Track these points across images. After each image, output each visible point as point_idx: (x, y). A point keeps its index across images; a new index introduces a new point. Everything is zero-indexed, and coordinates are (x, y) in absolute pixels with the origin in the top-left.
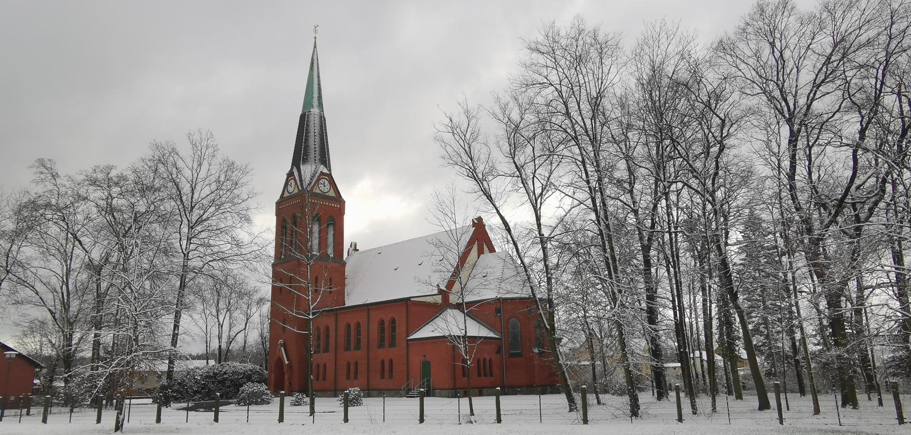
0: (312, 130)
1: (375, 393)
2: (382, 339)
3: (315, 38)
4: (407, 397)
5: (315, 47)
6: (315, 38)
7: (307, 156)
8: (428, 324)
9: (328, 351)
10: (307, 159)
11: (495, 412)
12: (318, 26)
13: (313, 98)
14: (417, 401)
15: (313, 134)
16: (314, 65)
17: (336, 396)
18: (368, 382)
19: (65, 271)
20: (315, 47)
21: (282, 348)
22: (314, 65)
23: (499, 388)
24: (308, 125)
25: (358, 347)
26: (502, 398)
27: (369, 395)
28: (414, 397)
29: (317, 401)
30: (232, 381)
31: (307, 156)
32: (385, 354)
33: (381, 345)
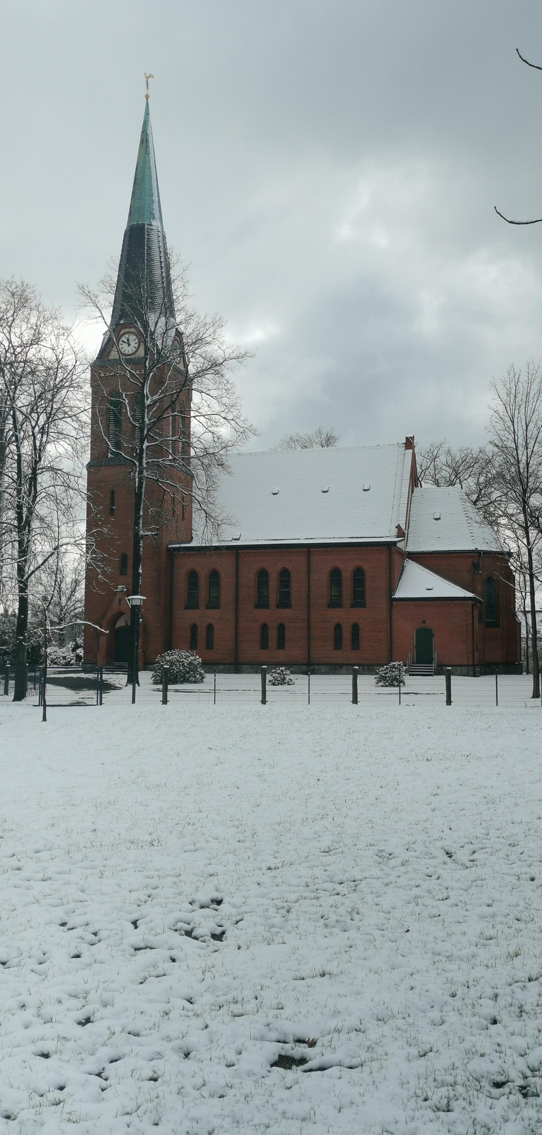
1: (323, 668)
3: (147, 97)
4: (410, 675)
5: (147, 114)
6: (147, 97)
12: (151, 76)
13: (153, 202)
20: (147, 114)
24: (149, 248)
28: (432, 675)
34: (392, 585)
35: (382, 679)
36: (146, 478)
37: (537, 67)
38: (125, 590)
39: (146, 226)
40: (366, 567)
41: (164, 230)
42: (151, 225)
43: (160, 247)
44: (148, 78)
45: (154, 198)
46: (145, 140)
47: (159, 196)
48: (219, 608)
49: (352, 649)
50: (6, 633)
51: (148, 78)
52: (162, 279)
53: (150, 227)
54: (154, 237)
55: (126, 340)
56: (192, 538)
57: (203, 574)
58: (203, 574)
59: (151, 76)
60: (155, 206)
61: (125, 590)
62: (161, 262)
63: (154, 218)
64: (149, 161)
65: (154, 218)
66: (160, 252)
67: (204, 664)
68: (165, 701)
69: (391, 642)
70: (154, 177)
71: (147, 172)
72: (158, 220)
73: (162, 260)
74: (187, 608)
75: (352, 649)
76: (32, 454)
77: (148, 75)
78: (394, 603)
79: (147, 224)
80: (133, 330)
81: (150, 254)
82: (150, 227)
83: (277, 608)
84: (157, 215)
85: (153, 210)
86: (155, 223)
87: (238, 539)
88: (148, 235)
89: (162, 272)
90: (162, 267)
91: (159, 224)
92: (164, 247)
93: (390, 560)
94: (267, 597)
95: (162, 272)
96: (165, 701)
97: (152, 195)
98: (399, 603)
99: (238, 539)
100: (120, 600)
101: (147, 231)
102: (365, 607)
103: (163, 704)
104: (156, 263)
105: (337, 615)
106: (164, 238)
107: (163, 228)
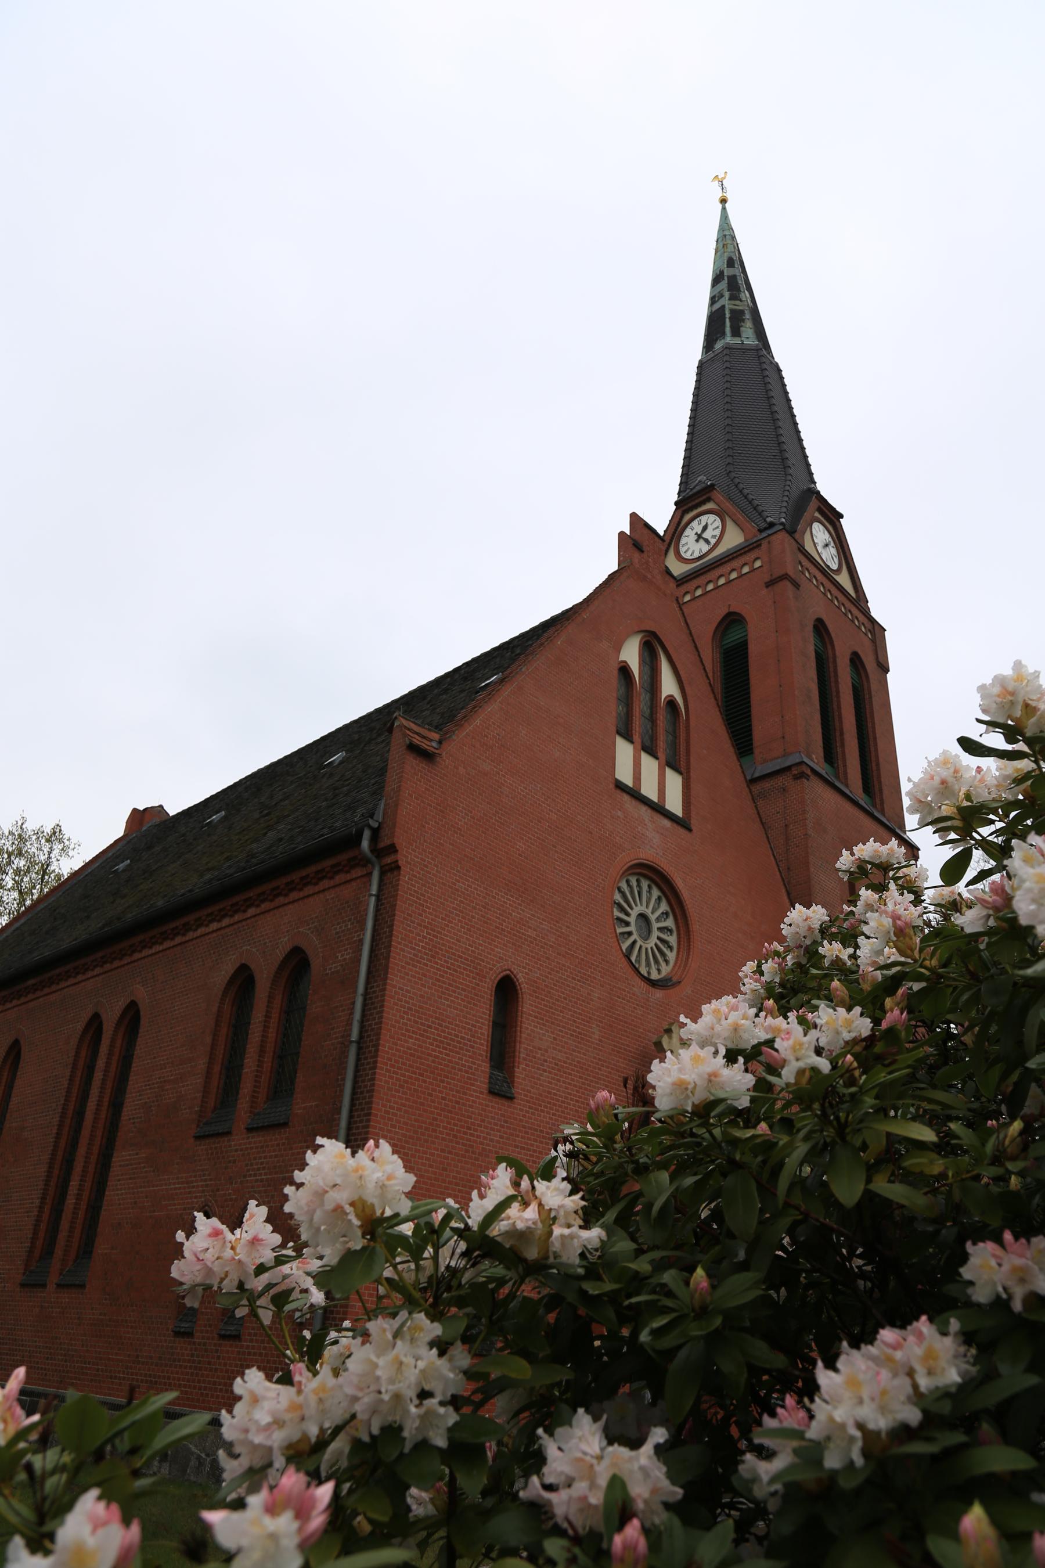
3: (723, 201)
16: (726, 238)
22: (726, 238)
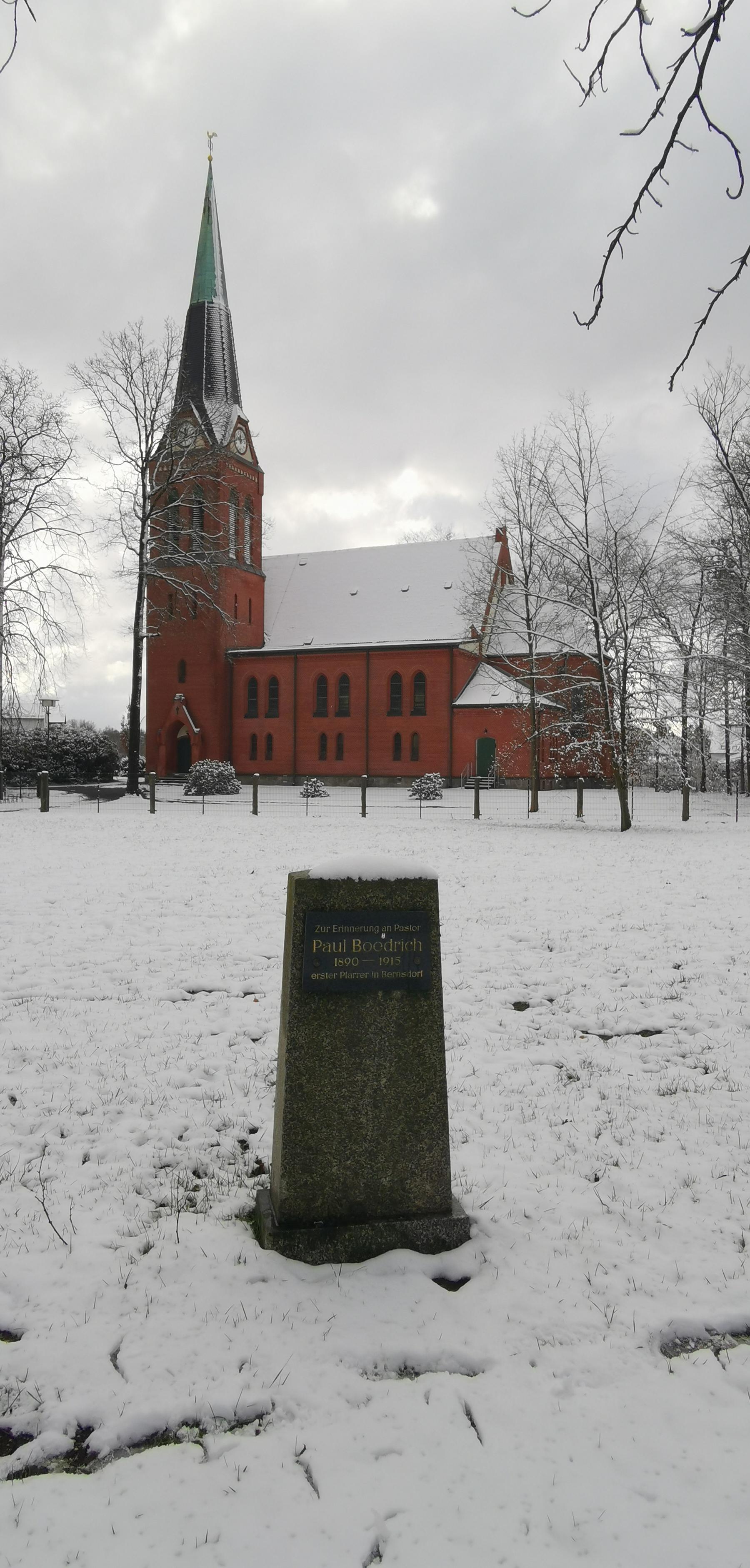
0: (218, 339)
1: (382, 781)
2: (253, 704)
3: (210, 159)
4: (466, 788)
5: (210, 178)
6: (210, 159)
7: (212, 383)
8: (468, 684)
9: (276, 715)
10: (212, 389)
11: (619, 812)
12: (214, 135)
13: (215, 277)
14: (472, 792)
15: (220, 345)
17: (296, 783)
18: (367, 766)
19: (144, 449)
20: (210, 178)
21: (184, 707)
23: (258, 775)
24: (210, 328)
25: (273, 710)
26: (586, 793)
27: (449, 785)
28: (487, 788)
29: (586, 793)
30: (75, 755)
31: (212, 385)
32: (404, 724)
33: (394, 708)
34: (455, 690)
35: (416, 792)
36: (148, 575)
37: (33, 15)
38: (183, 698)
39: (206, 304)
40: (427, 672)
41: (230, 307)
42: (212, 303)
43: (221, 326)
44: (211, 137)
45: (216, 273)
46: (207, 209)
47: (223, 271)
48: (278, 717)
49: (411, 760)
50: (68, 743)
51: (211, 137)
52: (224, 361)
53: (211, 305)
54: (215, 316)
55: (183, 431)
56: (264, 643)
57: (263, 680)
58: (263, 680)
59: (214, 135)
60: (218, 281)
61: (183, 698)
62: (223, 343)
63: (215, 295)
64: (212, 233)
65: (215, 295)
66: (222, 332)
67: (239, 775)
68: (153, 811)
69: (452, 753)
70: (217, 249)
71: (208, 245)
72: (221, 297)
73: (224, 341)
74: (246, 717)
75: (411, 760)
76: (649, 590)
77: (210, 134)
78: (455, 710)
79: (208, 302)
80: (190, 419)
81: (210, 335)
82: (211, 305)
83: (336, 716)
84: (219, 290)
85: (215, 285)
86: (218, 301)
87: (310, 644)
88: (209, 314)
89: (224, 354)
90: (223, 349)
91: (222, 302)
92: (229, 327)
93: (452, 664)
94: (348, 704)
95: (224, 354)
96: (153, 811)
97: (214, 269)
98: (460, 710)
99: (310, 644)
100: (178, 709)
101: (208, 310)
102: (425, 714)
103: (42, 811)
104: (217, 345)
105: (396, 724)
106: (228, 316)
107: (227, 306)
